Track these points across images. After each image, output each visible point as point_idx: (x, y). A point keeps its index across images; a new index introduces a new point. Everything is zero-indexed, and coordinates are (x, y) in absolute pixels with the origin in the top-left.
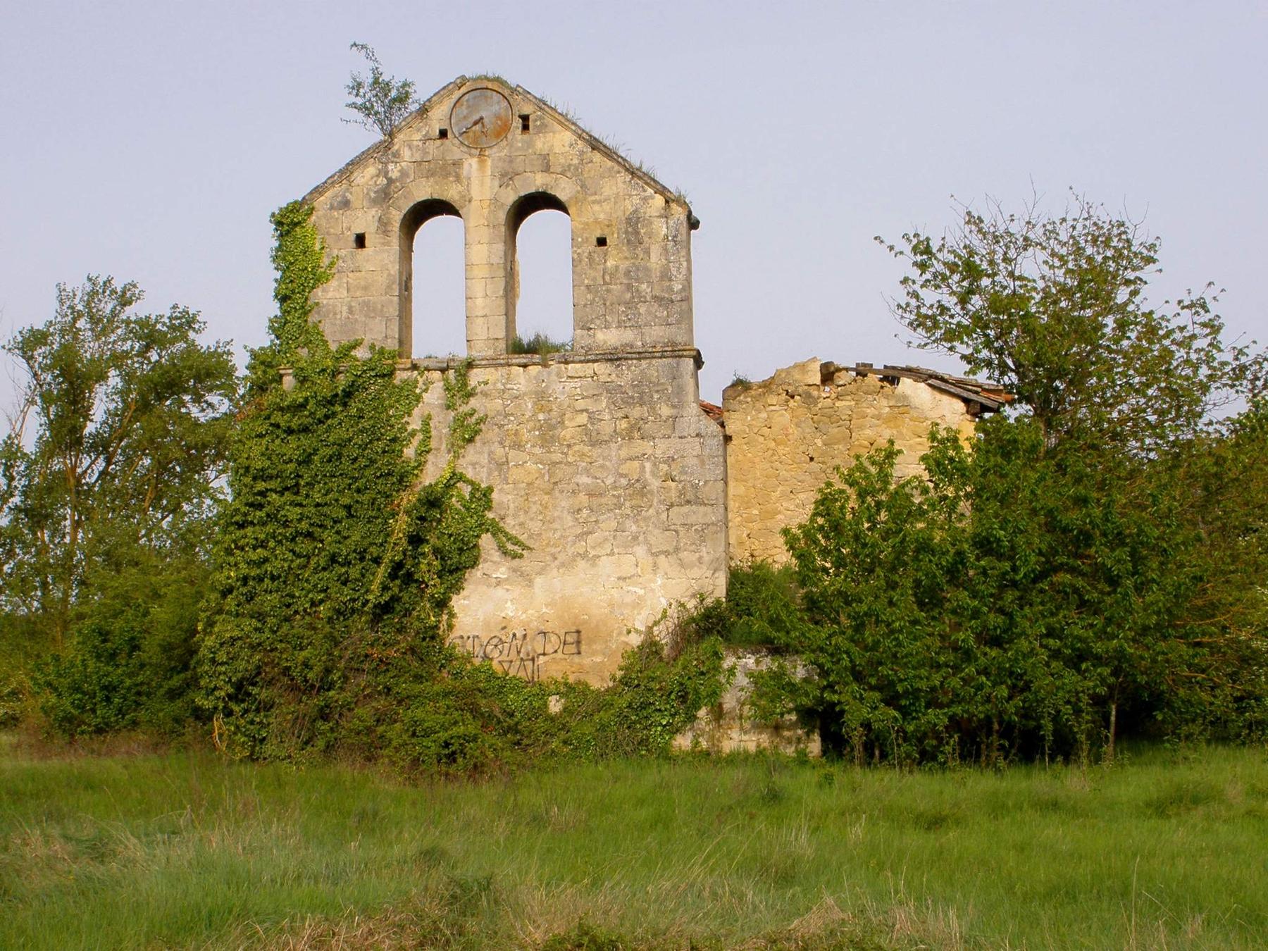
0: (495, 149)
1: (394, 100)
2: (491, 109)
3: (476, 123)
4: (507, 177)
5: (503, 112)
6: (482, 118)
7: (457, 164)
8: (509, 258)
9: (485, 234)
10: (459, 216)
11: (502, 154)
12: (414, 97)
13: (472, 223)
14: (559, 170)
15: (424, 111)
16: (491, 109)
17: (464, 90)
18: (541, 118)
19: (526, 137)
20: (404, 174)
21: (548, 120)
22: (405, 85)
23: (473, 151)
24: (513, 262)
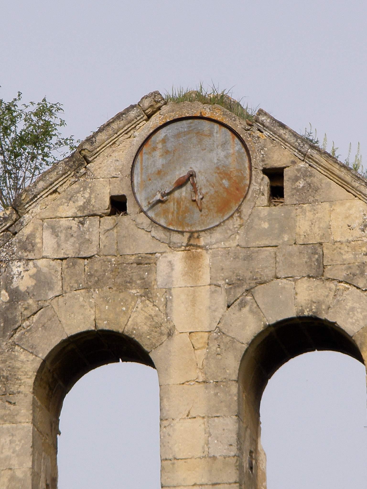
0: (217, 235)
1: (22, 140)
2: (210, 158)
3: (180, 184)
4: (240, 288)
5: (232, 164)
6: (192, 175)
7: (146, 262)
8: (247, 445)
9: (199, 399)
10: (149, 362)
11: (233, 244)
12: (62, 133)
13: (175, 377)
14: (342, 275)
15: (80, 160)
16: (210, 158)
17: (156, 120)
18: (305, 174)
19: (277, 210)
20: (42, 282)
21: (319, 178)
22: (44, 110)
23: (176, 238)
24: (254, 453)
